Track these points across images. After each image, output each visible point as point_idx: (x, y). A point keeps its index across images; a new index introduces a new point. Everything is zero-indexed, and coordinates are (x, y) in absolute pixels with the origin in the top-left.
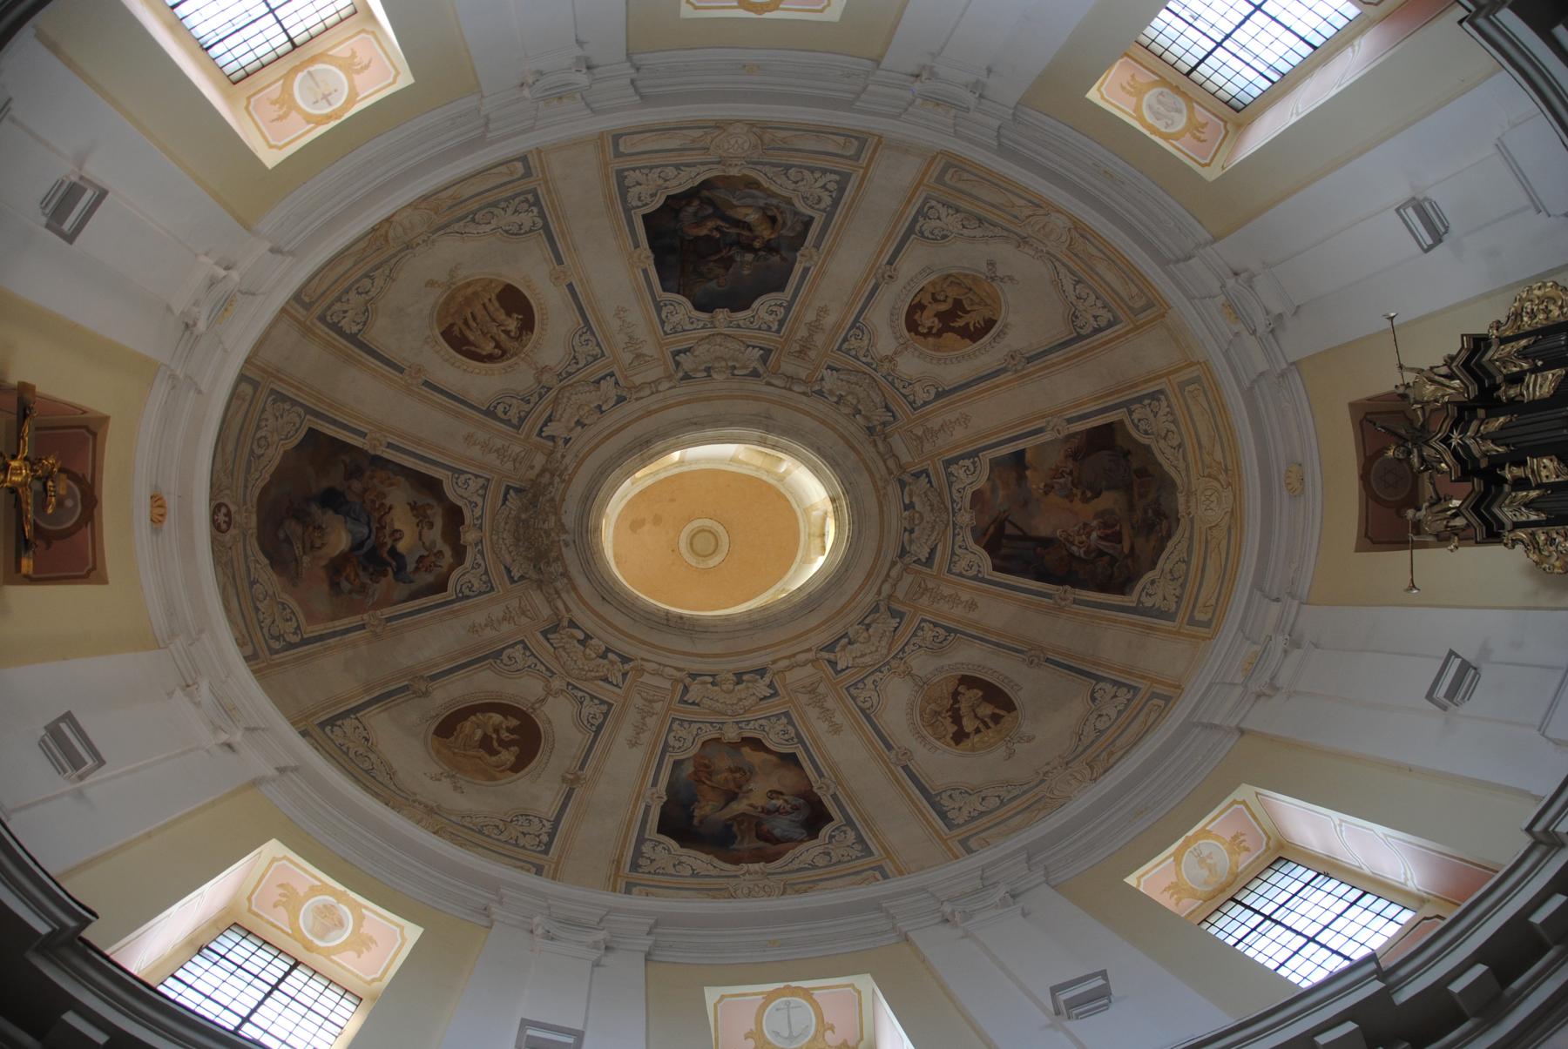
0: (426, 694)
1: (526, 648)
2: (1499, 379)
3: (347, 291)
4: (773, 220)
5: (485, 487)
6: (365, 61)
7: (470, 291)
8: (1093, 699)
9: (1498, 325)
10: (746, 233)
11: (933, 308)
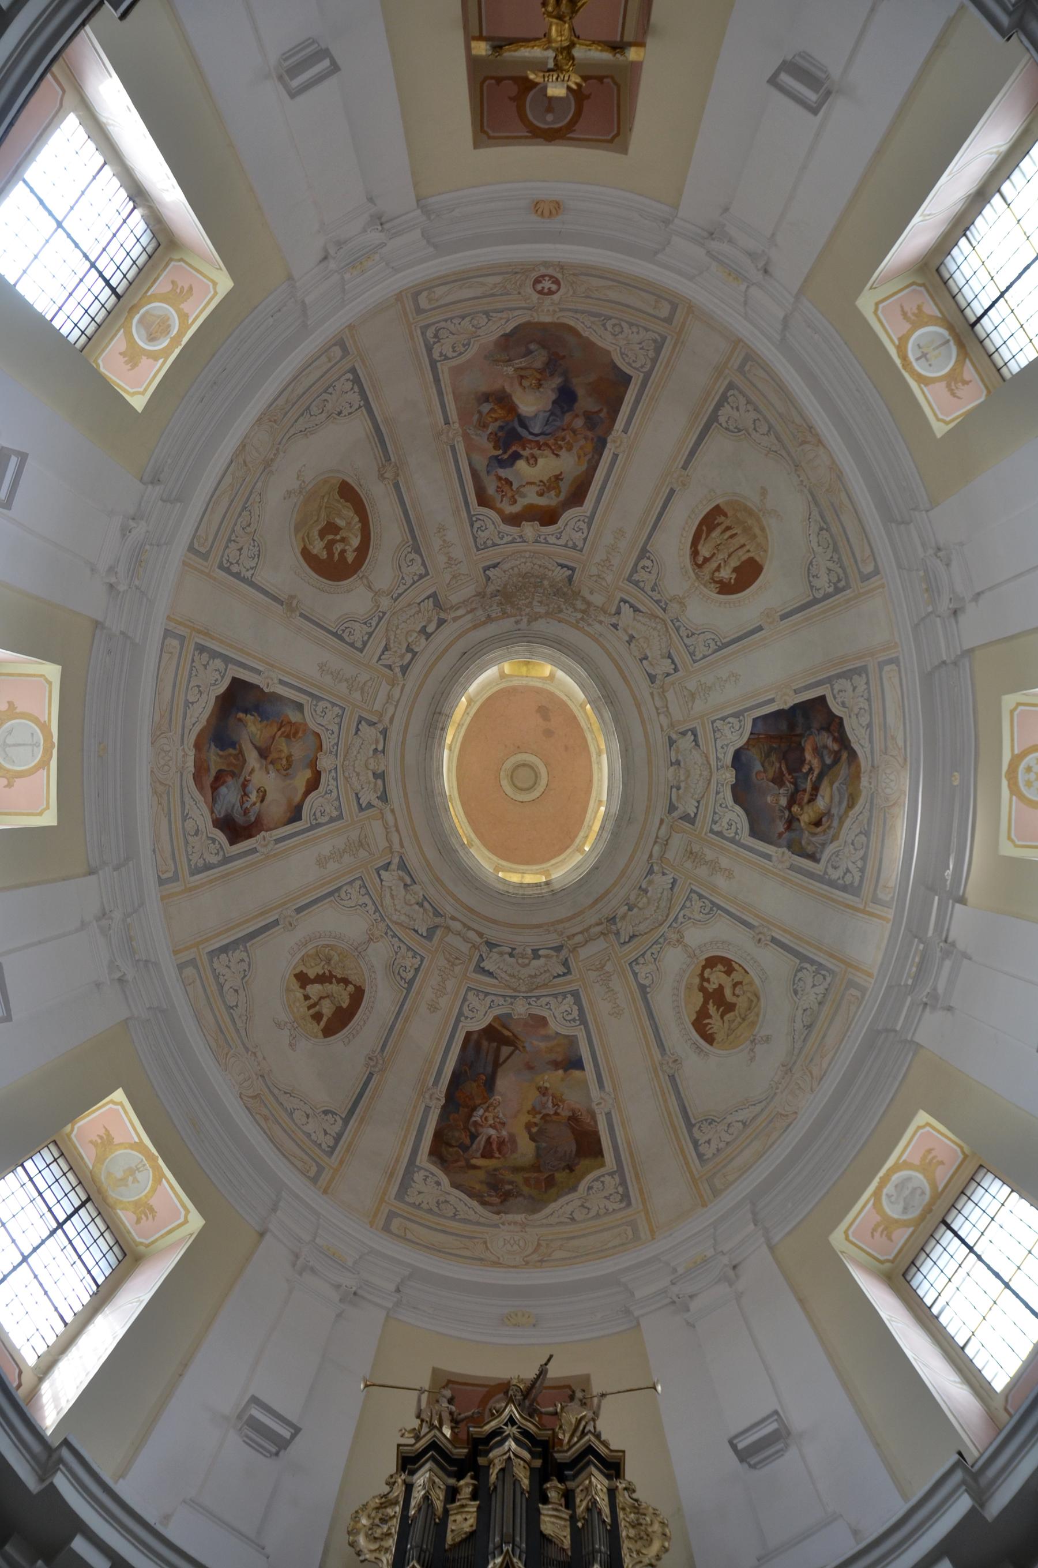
0: (382, 477)
1: (421, 577)
2: (571, 1485)
3: (756, 409)
4: (818, 823)
5: (574, 547)
6: (959, 393)
7: (757, 531)
8: (326, 1112)
9: (630, 1489)
10: (806, 798)
11: (727, 982)
